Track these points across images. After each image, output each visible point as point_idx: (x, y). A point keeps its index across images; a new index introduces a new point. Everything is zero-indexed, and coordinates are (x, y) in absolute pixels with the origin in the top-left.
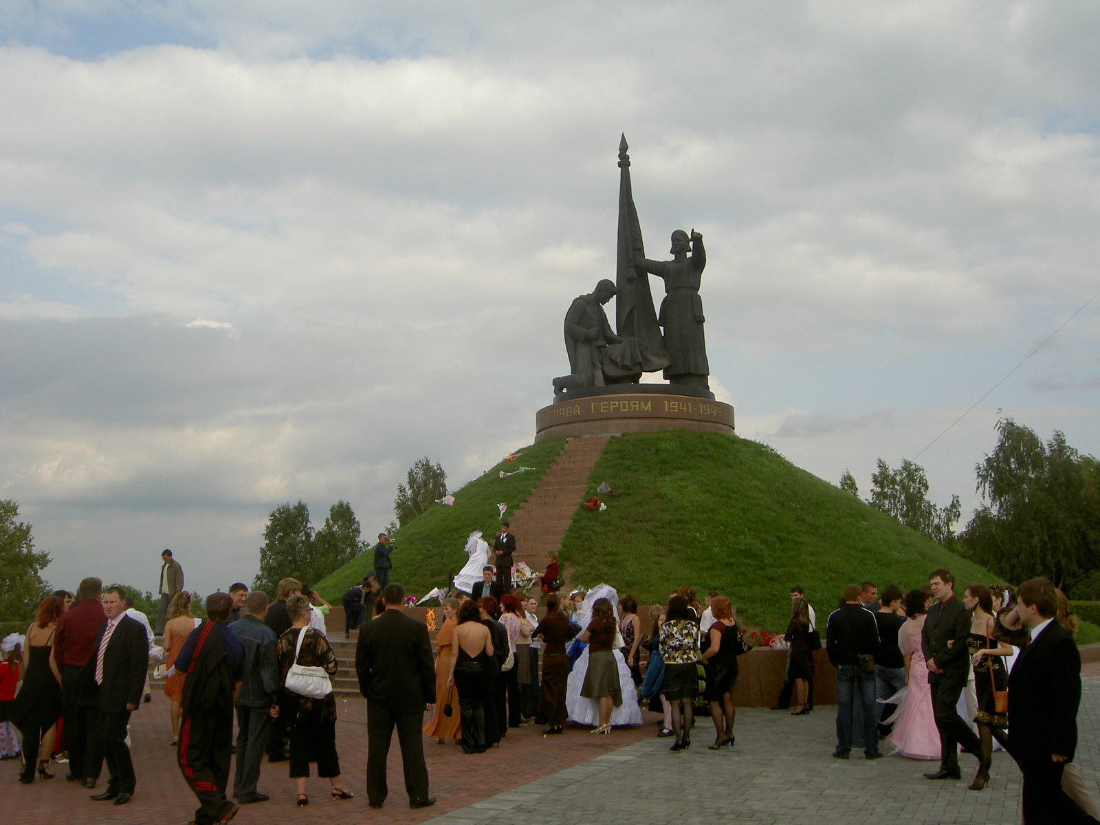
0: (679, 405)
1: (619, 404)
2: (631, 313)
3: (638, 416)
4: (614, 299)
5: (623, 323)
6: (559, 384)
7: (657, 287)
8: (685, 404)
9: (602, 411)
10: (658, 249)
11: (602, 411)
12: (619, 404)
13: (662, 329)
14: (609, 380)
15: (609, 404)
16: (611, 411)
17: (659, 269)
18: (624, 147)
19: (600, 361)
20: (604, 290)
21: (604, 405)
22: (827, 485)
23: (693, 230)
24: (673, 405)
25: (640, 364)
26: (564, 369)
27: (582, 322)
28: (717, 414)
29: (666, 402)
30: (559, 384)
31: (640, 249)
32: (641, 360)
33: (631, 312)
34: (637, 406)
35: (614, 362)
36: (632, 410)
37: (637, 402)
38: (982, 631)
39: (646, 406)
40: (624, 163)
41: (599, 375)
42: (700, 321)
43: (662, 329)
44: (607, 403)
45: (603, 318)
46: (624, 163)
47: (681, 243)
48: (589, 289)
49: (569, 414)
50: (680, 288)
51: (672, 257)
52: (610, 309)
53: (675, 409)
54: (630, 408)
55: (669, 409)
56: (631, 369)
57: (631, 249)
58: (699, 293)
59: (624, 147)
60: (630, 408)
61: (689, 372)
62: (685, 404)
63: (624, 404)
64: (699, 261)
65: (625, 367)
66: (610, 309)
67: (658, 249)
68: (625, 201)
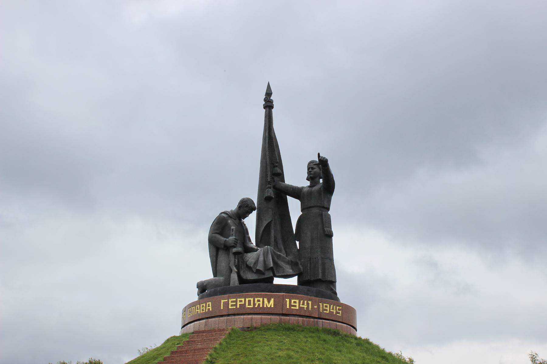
0: (299, 303)
1: (245, 301)
3: (260, 312)
4: (255, 213)
6: (203, 288)
7: (295, 208)
8: (306, 302)
9: (230, 307)
10: (296, 176)
11: (230, 307)
12: (245, 301)
13: (297, 243)
14: (242, 281)
15: (236, 301)
16: (238, 307)
17: (297, 193)
18: (269, 94)
19: (235, 266)
20: (245, 207)
21: (232, 302)
22: (211, 280)
24: (295, 302)
25: (272, 269)
26: (207, 274)
27: (225, 237)
28: (337, 313)
29: (288, 300)
30: (203, 288)
31: (281, 176)
33: (269, 225)
34: (261, 303)
35: (249, 268)
36: (256, 306)
37: (261, 299)
39: (269, 302)
40: (269, 105)
41: (234, 277)
43: (297, 243)
45: (244, 232)
46: (269, 105)
47: (315, 170)
48: (232, 206)
49: (203, 310)
50: (310, 207)
51: (308, 183)
52: (251, 222)
53: (295, 306)
54: (254, 304)
55: (290, 305)
56: (264, 274)
57: (269, 173)
59: (269, 94)
60: (254, 304)
62: (306, 302)
63: (249, 301)
64: (329, 187)
65: (258, 272)
66: (251, 222)
67: (296, 176)
68: (267, 134)
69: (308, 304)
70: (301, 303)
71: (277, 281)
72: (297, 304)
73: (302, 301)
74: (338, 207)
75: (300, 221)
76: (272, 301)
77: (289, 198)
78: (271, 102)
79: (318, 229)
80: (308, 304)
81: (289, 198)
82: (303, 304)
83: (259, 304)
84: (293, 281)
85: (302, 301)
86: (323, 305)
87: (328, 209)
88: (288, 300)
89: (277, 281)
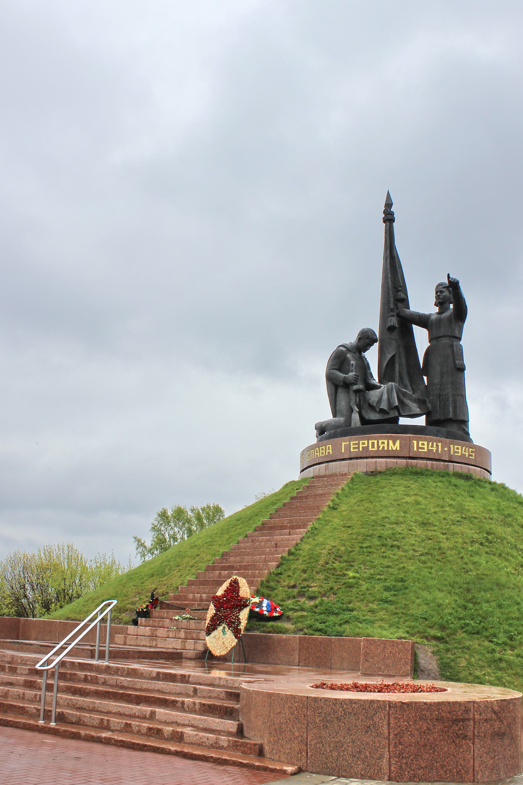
1: (368, 443)
2: (392, 360)
3: (386, 455)
5: (383, 370)
7: (421, 338)
8: (435, 444)
10: (422, 301)
11: (352, 450)
12: (368, 443)
13: (425, 378)
14: (364, 421)
15: (359, 444)
16: (361, 449)
17: (423, 321)
18: (389, 205)
20: (366, 340)
21: (354, 444)
23: (448, 275)
25: (397, 408)
28: (470, 455)
29: (415, 442)
31: (405, 301)
32: (397, 404)
34: (386, 445)
35: (372, 407)
36: (381, 449)
37: (386, 441)
38: (230, 634)
39: (394, 444)
40: (389, 218)
41: (356, 417)
42: (461, 369)
43: (425, 378)
44: (357, 442)
46: (389, 218)
51: (437, 309)
52: (372, 356)
53: (423, 448)
54: (378, 447)
55: (418, 448)
57: (392, 299)
58: (461, 343)
59: (389, 205)
60: (378, 447)
61: (449, 421)
63: (373, 444)
65: (382, 411)
66: (372, 356)
67: (422, 301)
69: (437, 446)
70: (463, 450)
71: (403, 421)
72: (426, 447)
73: (430, 443)
74: (473, 339)
75: (428, 353)
76: (398, 443)
77: (413, 325)
78: (392, 214)
79: (449, 365)
80: (437, 446)
81: (413, 325)
82: (432, 446)
83: (384, 447)
84: (421, 421)
85: (430, 443)
86: (454, 447)
87: (460, 339)
88: (415, 442)
89: (403, 421)
